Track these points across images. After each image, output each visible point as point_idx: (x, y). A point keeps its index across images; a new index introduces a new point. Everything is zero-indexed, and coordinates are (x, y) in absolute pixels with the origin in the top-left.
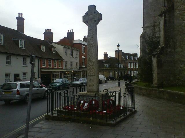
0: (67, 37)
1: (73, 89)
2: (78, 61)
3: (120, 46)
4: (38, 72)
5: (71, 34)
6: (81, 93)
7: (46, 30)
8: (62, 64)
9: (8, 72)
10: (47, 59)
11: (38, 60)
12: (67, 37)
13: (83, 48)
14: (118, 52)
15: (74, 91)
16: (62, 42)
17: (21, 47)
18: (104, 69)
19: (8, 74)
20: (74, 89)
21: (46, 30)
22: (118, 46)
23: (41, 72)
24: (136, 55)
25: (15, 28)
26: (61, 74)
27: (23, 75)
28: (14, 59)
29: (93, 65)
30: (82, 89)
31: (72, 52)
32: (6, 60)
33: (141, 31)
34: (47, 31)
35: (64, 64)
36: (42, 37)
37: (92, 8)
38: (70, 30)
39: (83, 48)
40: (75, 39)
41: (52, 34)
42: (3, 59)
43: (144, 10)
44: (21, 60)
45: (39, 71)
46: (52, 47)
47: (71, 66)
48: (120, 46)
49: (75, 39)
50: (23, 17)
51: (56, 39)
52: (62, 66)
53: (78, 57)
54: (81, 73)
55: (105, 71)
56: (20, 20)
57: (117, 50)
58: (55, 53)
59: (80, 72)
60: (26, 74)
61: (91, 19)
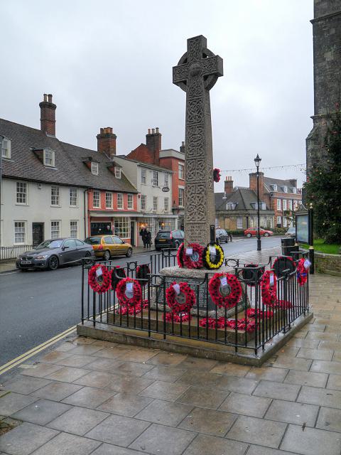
0: (145, 144)
1: (151, 259)
2: (169, 195)
3: (260, 160)
4: (85, 219)
5: (154, 138)
6: (168, 268)
7: (101, 129)
8: (135, 201)
9: (20, 218)
10: (103, 191)
11: (85, 193)
12: (145, 144)
13: (180, 168)
14: (256, 177)
15: (153, 262)
16: (137, 155)
17: (48, 165)
18: (226, 213)
19: (20, 223)
20: (153, 257)
21: (101, 129)
22: (258, 160)
23: (91, 218)
24: (293, 183)
25: (37, 125)
26: (132, 223)
27: (52, 225)
28: (32, 192)
29: (200, 196)
30: (172, 258)
31: (143, 173)
32: (51, 196)
33: (310, 126)
34: (105, 132)
35: (139, 201)
36: (93, 146)
37: (197, 44)
38: (153, 129)
39: (180, 168)
40: (163, 147)
41: (115, 137)
42: (10, 189)
43: (317, 77)
44: (47, 191)
45: (87, 217)
46: (114, 164)
47: (155, 205)
48: (260, 160)
49: (162, 149)
50: (53, 102)
51: (123, 147)
52: (135, 207)
53: (170, 186)
54: (177, 221)
55: (228, 218)
56: (48, 108)
57: (255, 171)
58: (120, 177)
59: (174, 218)
60: (23, 223)
61: (195, 74)
